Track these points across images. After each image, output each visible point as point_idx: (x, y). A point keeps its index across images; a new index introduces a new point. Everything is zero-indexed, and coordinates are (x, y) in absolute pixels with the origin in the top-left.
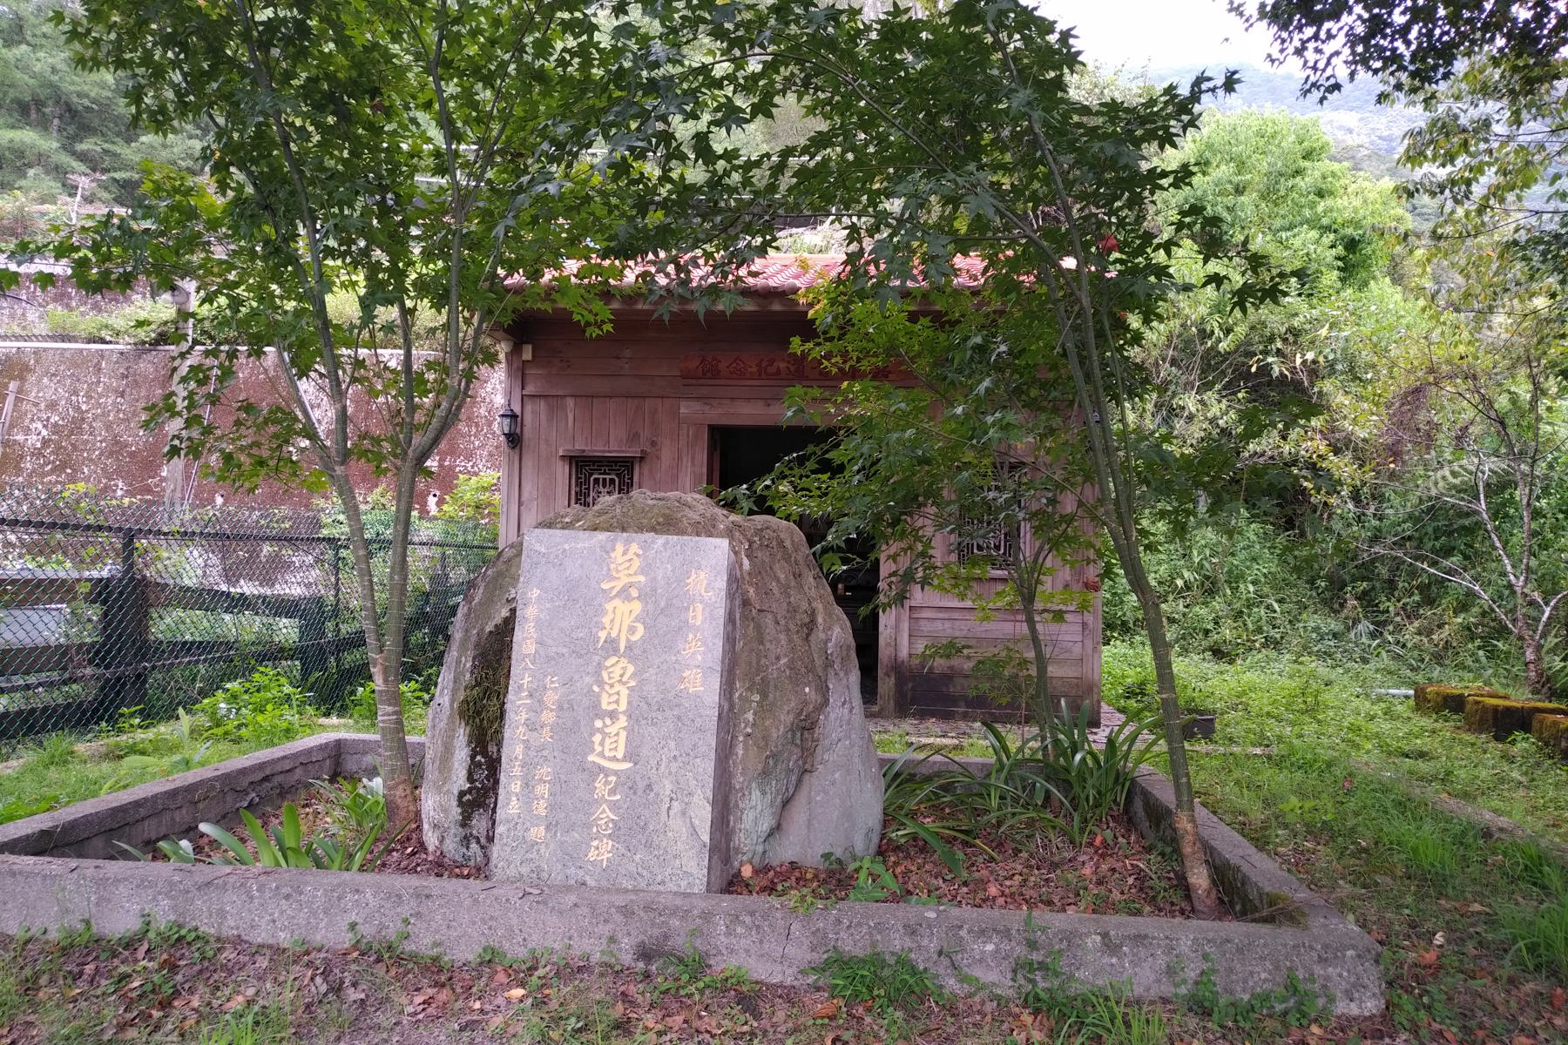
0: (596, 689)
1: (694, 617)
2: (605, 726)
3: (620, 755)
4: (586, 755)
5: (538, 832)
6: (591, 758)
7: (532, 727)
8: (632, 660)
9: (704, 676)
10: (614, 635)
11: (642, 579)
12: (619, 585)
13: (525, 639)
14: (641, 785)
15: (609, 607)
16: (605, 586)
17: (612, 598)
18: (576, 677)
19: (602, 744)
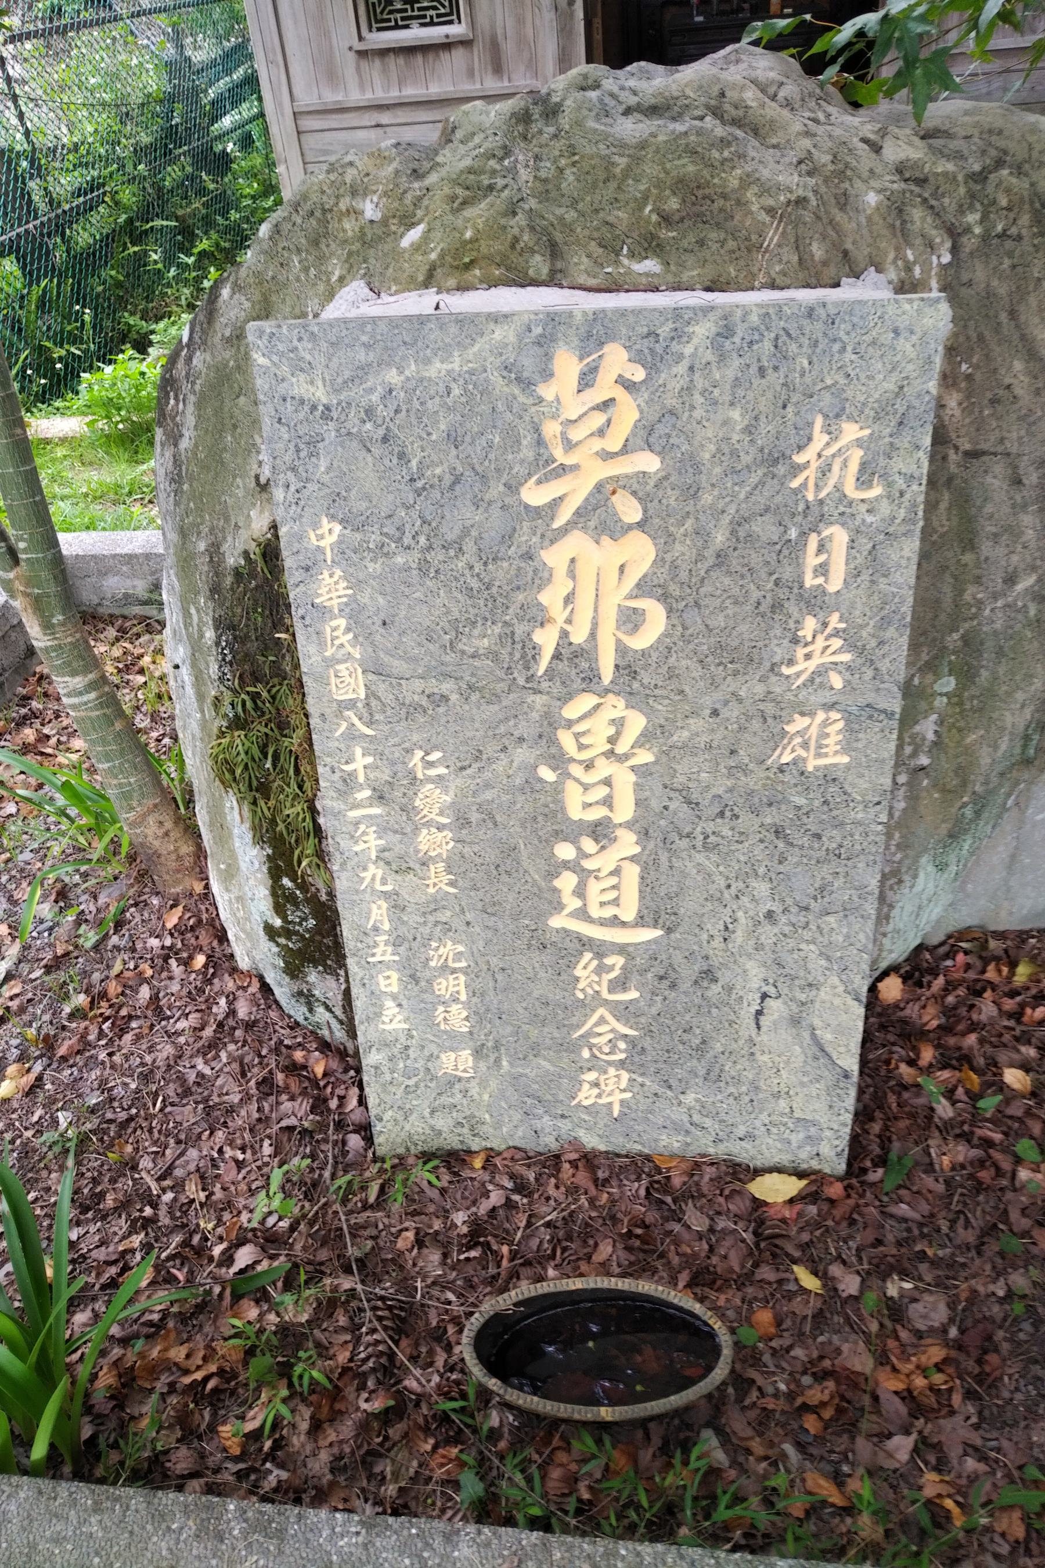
0: (547, 774)
1: (823, 570)
2: (582, 854)
3: (629, 914)
4: (542, 916)
5: (458, 1062)
6: (556, 922)
7: (400, 864)
8: (633, 699)
9: (851, 729)
10: (579, 636)
11: (649, 463)
12: (576, 490)
13: (331, 662)
14: (688, 972)
15: (555, 557)
16: (535, 495)
17: (564, 531)
18: (491, 749)
19: (580, 892)
